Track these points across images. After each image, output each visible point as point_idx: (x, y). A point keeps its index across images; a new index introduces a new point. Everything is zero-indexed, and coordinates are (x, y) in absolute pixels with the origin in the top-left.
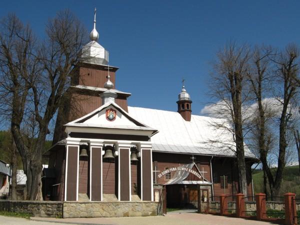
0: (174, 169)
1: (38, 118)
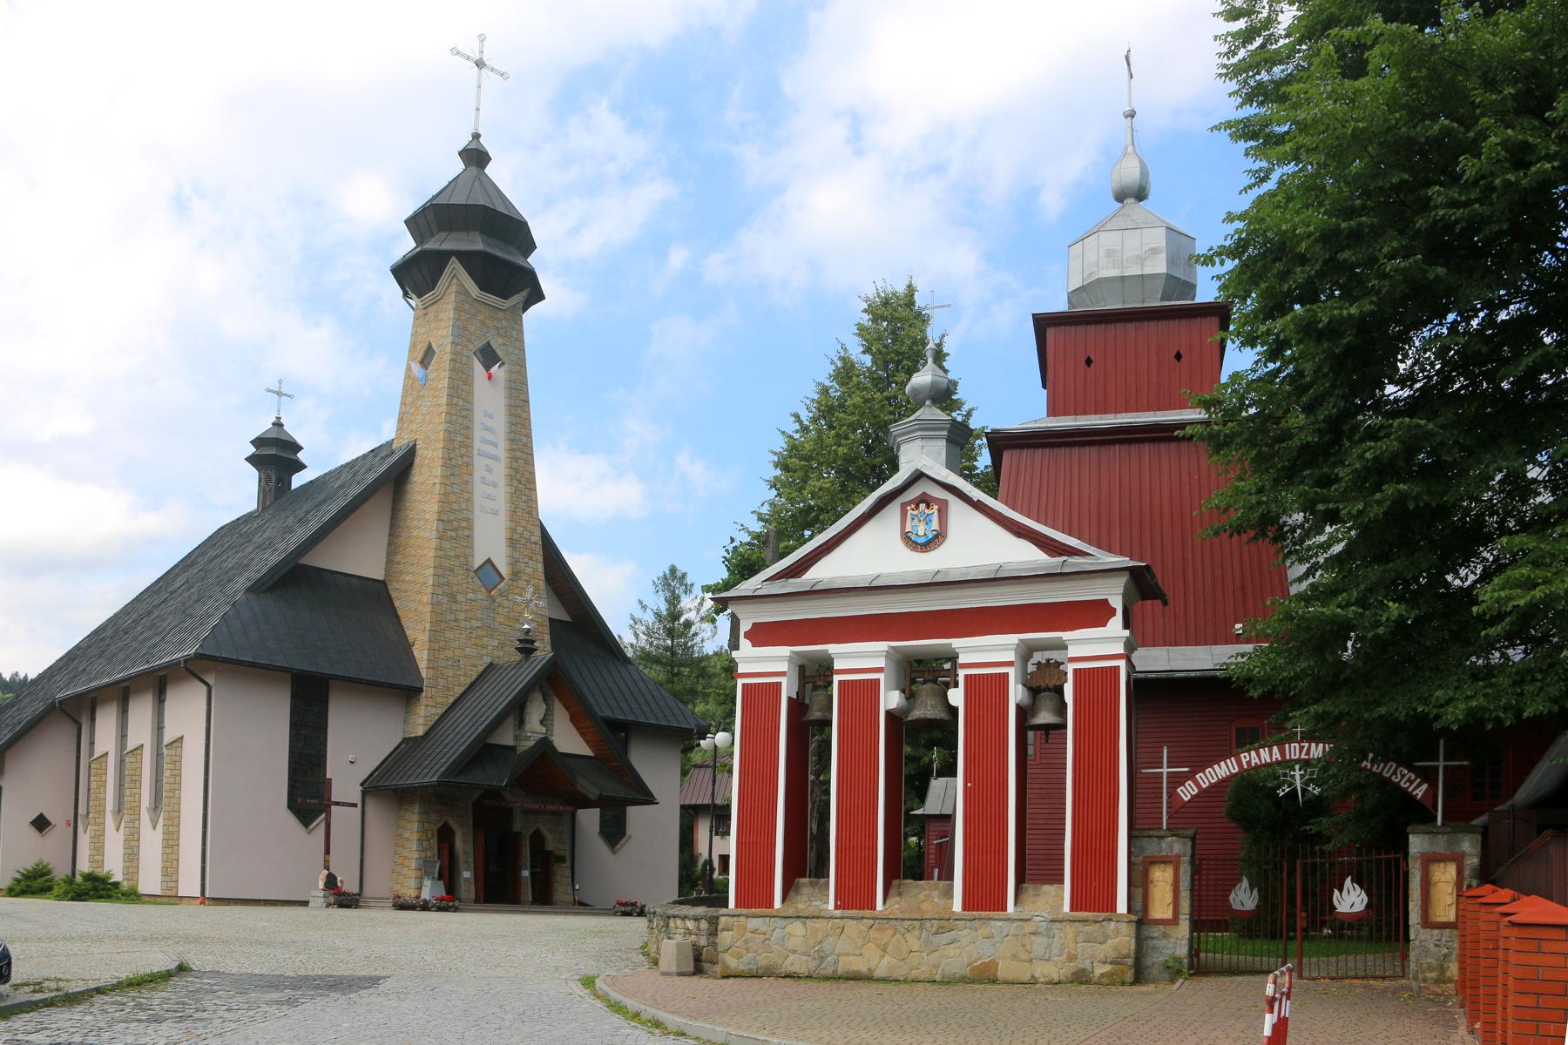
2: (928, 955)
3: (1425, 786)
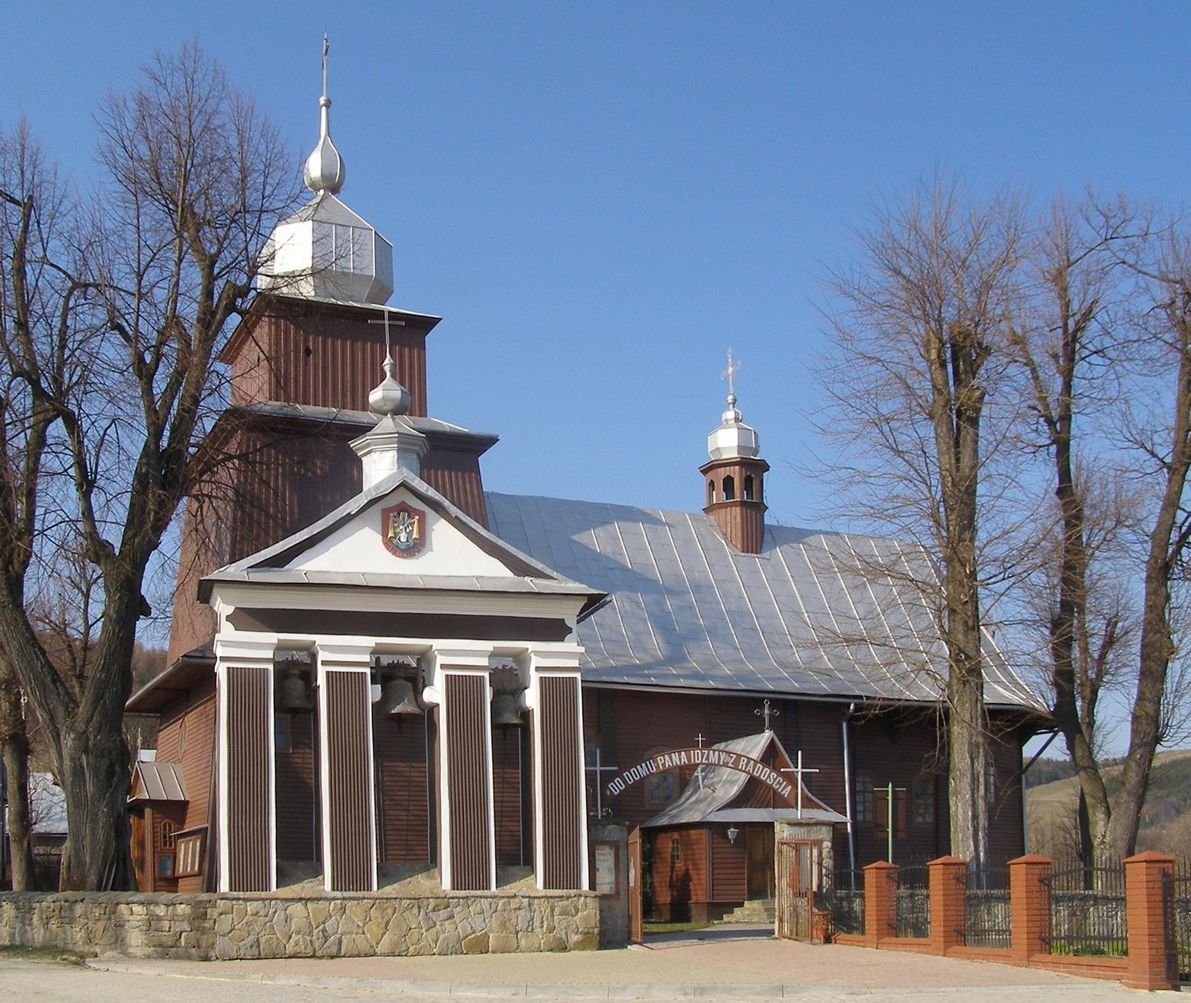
0: (675, 757)
1: (98, 550)
2: (427, 931)
3: (790, 787)
